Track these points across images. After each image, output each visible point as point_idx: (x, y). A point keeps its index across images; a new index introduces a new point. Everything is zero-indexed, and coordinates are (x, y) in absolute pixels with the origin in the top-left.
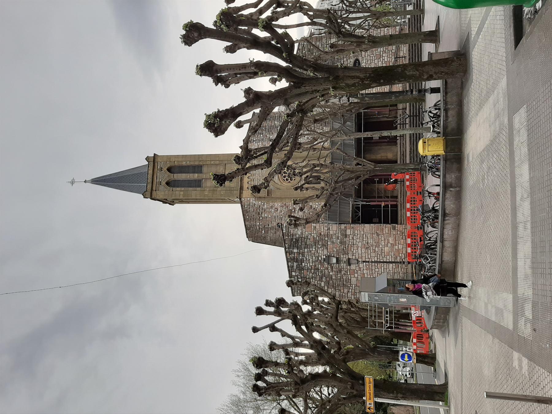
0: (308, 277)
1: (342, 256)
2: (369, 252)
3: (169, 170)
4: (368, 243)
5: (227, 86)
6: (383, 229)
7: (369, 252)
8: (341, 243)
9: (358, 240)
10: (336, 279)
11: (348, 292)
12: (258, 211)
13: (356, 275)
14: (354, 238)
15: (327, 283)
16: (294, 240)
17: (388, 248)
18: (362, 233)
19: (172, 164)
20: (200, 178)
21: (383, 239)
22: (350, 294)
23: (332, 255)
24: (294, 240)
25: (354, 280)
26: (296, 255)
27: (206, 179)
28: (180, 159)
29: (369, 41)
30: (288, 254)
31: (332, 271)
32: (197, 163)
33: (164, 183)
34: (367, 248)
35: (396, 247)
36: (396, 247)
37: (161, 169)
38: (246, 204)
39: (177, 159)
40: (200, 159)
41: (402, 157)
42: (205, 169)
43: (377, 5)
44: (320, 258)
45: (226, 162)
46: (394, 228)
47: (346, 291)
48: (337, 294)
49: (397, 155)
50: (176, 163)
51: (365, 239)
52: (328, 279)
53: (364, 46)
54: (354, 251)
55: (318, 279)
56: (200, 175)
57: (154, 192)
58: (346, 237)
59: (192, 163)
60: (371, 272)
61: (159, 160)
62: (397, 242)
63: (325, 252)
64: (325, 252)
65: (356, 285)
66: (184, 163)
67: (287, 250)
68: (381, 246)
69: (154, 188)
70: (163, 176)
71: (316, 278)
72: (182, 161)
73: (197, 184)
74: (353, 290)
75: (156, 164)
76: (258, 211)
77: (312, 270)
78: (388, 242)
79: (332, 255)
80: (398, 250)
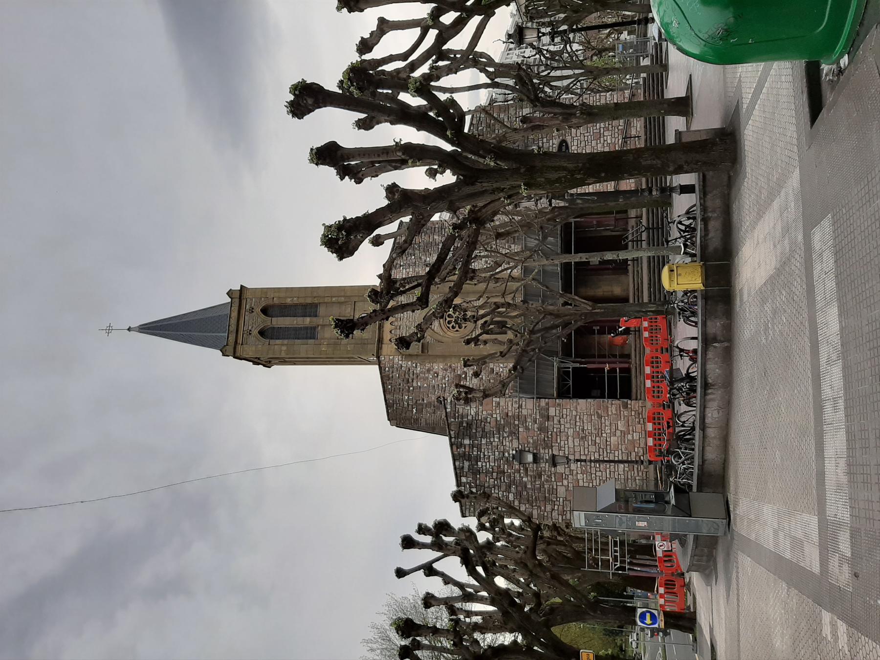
0: (486, 485)
1: (542, 451)
2: (586, 445)
3: (265, 311)
4: (583, 430)
5: (359, 181)
6: (607, 407)
7: (586, 445)
8: (540, 429)
9: (568, 426)
10: (533, 489)
11: (553, 510)
12: (407, 376)
13: (565, 482)
14: (562, 422)
15: (519, 495)
16: (465, 425)
17: (616, 438)
18: (574, 413)
19: (270, 302)
20: (314, 324)
21: (607, 423)
22: (555, 514)
23: (527, 449)
24: (465, 425)
25: (561, 491)
26: (467, 450)
27: (323, 326)
28: (282, 295)
29: (582, 113)
30: (455, 447)
31: (527, 476)
32: (309, 301)
33: (255, 332)
34: (582, 438)
35: (630, 437)
36: (630, 437)
37: (252, 310)
38: (387, 365)
39: (277, 295)
40: (315, 294)
41: (636, 293)
42: (322, 310)
43: (595, 58)
44: (506, 454)
45: (356, 299)
46: (626, 406)
47: (549, 508)
48: (535, 513)
49: (628, 290)
50: (276, 301)
51: (578, 424)
52: (519, 489)
53: (574, 121)
54: (562, 443)
55: (503, 488)
56: (314, 319)
57: (239, 347)
58: (548, 420)
59: (302, 301)
60: (589, 478)
61: (247, 295)
62: (631, 428)
63: (515, 444)
64: (515, 444)
65: (565, 499)
66: (289, 301)
67: (453, 440)
68: (604, 435)
69: (240, 341)
70: (255, 321)
71: (499, 487)
72: (286, 298)
73: (310, 333)
74: (561, 507)
75: (244, 302)
76: (407, 376)
77: (495, 474)
78: (617, 429)
79: (527, 449)
80: (633, 442)
